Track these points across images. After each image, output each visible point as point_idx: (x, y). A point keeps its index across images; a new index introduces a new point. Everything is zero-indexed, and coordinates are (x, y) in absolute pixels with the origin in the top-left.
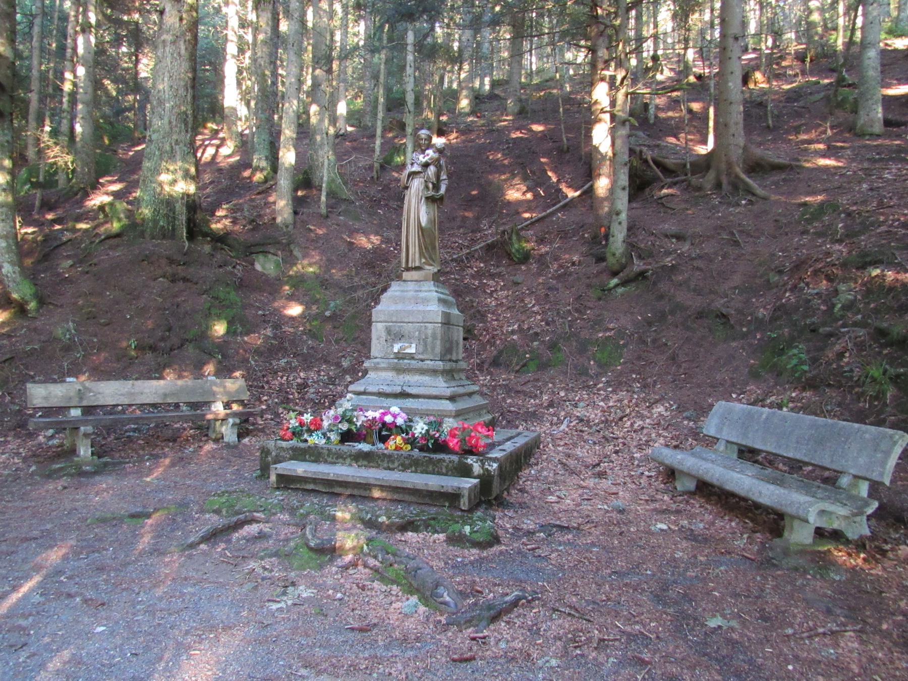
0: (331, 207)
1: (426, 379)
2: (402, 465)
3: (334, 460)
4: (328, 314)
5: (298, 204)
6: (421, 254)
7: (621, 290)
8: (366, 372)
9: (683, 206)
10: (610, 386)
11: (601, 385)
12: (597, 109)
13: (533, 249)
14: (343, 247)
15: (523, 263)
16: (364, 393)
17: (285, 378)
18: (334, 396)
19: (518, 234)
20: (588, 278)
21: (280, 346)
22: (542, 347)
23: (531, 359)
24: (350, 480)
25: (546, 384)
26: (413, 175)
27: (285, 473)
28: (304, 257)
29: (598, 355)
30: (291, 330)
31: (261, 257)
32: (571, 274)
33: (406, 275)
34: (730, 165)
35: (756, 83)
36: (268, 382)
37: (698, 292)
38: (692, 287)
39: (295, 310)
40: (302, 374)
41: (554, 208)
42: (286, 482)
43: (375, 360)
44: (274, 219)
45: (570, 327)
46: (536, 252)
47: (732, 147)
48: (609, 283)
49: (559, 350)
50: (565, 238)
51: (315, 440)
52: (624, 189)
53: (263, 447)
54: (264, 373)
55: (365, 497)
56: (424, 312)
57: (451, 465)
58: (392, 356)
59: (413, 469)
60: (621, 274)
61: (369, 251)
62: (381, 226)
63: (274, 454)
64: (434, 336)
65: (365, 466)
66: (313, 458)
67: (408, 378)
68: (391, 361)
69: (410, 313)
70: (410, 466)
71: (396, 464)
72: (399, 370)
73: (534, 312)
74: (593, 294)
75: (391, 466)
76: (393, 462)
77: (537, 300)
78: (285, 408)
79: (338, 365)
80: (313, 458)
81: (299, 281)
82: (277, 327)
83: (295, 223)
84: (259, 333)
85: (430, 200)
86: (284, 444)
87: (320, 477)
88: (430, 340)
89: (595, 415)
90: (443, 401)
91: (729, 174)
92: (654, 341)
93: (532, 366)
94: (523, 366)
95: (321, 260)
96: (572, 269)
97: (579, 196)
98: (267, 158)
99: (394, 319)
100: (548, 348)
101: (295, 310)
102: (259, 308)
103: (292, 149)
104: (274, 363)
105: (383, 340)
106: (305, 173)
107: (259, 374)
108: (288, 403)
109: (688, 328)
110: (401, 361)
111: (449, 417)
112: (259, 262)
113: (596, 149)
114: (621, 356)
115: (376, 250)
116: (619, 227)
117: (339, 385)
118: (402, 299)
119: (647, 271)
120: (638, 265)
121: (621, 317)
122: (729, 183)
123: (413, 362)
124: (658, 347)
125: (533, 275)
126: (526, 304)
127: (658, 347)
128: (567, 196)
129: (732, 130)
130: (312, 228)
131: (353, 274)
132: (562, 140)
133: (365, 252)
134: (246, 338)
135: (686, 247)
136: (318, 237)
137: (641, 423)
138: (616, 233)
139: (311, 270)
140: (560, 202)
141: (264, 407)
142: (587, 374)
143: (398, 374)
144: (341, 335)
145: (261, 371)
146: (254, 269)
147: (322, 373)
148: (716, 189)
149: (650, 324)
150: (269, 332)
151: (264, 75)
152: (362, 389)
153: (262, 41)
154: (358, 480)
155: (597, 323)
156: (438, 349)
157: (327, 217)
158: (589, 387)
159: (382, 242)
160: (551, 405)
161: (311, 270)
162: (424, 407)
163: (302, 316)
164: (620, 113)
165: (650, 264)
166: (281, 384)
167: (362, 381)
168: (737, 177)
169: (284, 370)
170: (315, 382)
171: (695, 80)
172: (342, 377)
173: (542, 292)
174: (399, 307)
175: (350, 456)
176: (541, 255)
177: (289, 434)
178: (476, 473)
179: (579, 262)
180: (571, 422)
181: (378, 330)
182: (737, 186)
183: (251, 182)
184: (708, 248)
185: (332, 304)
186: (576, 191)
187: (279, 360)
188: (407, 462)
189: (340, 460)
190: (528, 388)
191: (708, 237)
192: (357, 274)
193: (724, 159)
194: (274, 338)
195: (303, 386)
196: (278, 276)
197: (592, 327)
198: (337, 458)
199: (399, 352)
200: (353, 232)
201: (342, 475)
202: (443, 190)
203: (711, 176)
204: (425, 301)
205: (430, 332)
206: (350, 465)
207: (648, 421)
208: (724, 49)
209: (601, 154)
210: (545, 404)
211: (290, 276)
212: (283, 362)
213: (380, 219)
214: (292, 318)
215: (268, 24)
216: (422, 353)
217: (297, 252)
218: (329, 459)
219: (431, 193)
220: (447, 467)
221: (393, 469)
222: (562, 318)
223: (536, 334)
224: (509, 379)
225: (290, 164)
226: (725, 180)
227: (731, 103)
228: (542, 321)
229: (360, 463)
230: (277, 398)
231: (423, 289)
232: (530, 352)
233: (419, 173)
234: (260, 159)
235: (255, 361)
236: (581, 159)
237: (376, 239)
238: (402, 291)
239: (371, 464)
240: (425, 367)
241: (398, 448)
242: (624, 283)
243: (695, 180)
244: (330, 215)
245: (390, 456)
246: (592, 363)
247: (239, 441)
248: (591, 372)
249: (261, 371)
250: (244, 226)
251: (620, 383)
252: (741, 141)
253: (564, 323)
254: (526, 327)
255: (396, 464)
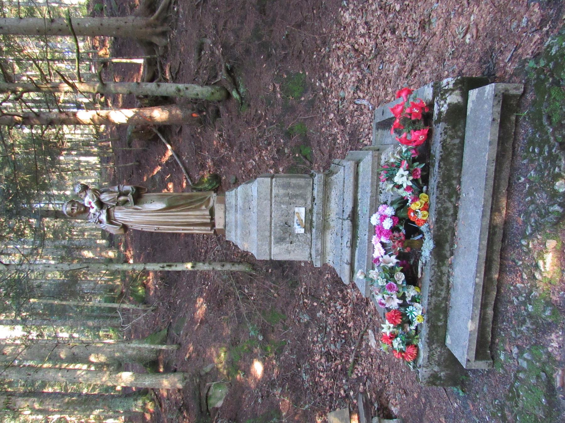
0: (173, 342)
1: (334, 194)
2: (450, 196)
3: (444, 288)
4: (261, 338)
5: (170, 370)
6: (197, 208)
7: (242, 90)
8: (325, 265)
9: (178, 56)
10: (324, 75)
11: (323, 85)
12: (98, 119)
13: (210, 171)
14: (204, 328)
15: (221, 179)
16: (352, 265)
17: (321, 374)
18: (337, 325)
19: (198, 185)
20: (232, 120)
21: (290, 379)
22: (289, 144)
23: (300, 152)
24: (484, 254)
25: (322, 134)
26: (110, 219)
27: (474, 347)
28: (212, 361)
29: (296, 94)
30: (276, 371)
31: (211, 401)
32: (229, 136)
33: (219, 225)
34: (148, 25)
35: (106, 54)
36: (326, 391)
37: (244, 18)
38: (239, 26)
39: (258, 368)
40: (317, 358)
41: (179, 162)
42: (485, 346)
43: (313, 253)
44: (179, 390)
45: (272, 124)
46: (212, 170)
47: (135, 23)
48: (236, 99)
49: (292, 129)
50: (201, 148)
51: (417, 313)
52: (159, 86)
53: (428, 382)
54: (317, 395)
55: (505, 236)
56: (259, 198)
57: (450, 132)
58: (309, 236)
59: (454, 182)
60: (229, 89)
61: (208, 306)
62: (189, 300)
63: (436, 369)
64: (286, 186)
65: (452, 245)
66: (442, 316)
67: (333, 216)
68: (314, 236)
69: (260, 214)
70: (450, 186)
71: (449, 205)
72: (324, 227)
73: (259, 159)
74: (245, 111)
75: (451, 212)
76: (447, 209)
77: (250, 158)
78: (352, 372)
79: (307, 325)
80: (442, 316)
81: (233, 365)
82: (272, 385)
83: (183, 372)
84: (279, 401)
85: (138, 198)
86: (423, 355)
87: (480, 297)
88: (290, 191)
89: (352, 77)
90: (361, 169)
91: (155, 26)
92: (284, 48)
93: (306, 151)
94: (305, 157)
95: (214, 346)
96: (225, 136)
97: (171, 146)
98: (136, 400)
99: (267, 234)
100: (290, 139)
101: (258, 368)
102: (256, 401)
103: (119, 374)
104: (306, 385)
105: (291, 247)
106: (145, 365)
107: (318, 400)
108: (346, 369)
109: (273, 21)
110: (314, 224)
111: (379, 159)
112: (214, 404)
113: (130, 120)
114: (298, 74)
115: (207, 301)
116: (190, 89)
117: (326, 322)
118: (245, 227)
119: (226, 68)
120: (222, 76)
121: (266, 82)
122: (162, 25)
123: (315, 211)
124: (289, 43)
125: (229, 168)
126: (253, 167)
127: (289, 43)
128: (171, 156)
129: (123, 24)
130: (188, 356)
131: (226, 317)
132: (132, 166)
133: (209, 308)
134: (284, 414)
135: (208, 41)
136: (195, 350)
137: (361, 27)
138: (195, 92)
139: (222, 355)
140: (175, 160)
141: (352, 393)
142: (313, 101)
143: (329, 228)
144: (280, 325)
145: (315, 398)
146: (221, 407)
147: (315, 339)
148: (166, 35)
149: (269, 56)
150: (278, 391)
151: (68, 403)
152: (347, 268)
153: (40, 405)
154: (485, 243)
155: (269, 102)
156: (302, 182)
157: (180, 344)
158: (325, 95)
159: (201, 296)
160: (342, 122)
161: (222, 355)
162: (368, 190)
163: (263, 361)
164: (96, 88)
165: (221, 65)
166: (327, 377)
167: (338, 270)
168: (157, 19)
169: (313, 375)
170: (324, 346)
171: (104, 97)
172: (319, 320)
173: (243, 154)
174: (253, 228)
175: (439, 266)
176: (214, 165)
177: (411, 350)
178: (460, 99)
179: (219, 131)
180: (359, 98)
181: (279, 253)
182: (164, 20)
183: (154, 413)
184: (209, 22)
185: (252, 333)
186: (167, 148)
187: (303, 381)
188: (446, 191)
189: (445, 278)
190: (326, 149)
191: (200, 25)
192: (227, 314)
193: (144, 30)
194: (283, 387)
195: (328, 356)
196: (227, 385)
197: (272, 105)
198: (442, 284)
199: (305, 227)
200: (193, 321)
201: (478, 266)
202: (128, 188)
203: (156, 40)
204: (247, 199)
205: (282, 192)
206: (451, 266)
207: (358, 22)
208: (60, 30)
209: (135, 115)
210: (342, 128)
211: (228, 374)
212: (306, 377)
213: (185, 301)
214: (265, 370)
215: (27, 400)
216: (306, 200)
217: (208, 369)
218: (443, 294)
219: (130, 198)
220: (452, 138)
221: (456, 209)
222: (264, 133)
223: (278, 151)
224: (318, 168)
225: (132, 376)
226: (160, 29)
227: (101, 25)
228: (267, 149)
229: (448, 254)
230: (342, 380)
231: (234, 202)
232: (294, 154)
233: (108, 212)
234: (136, 405)
235: (305, 404)
236: (145, 150)
237: (200, 301)
238: (236, 226)
239: (449, 238)
240: (321, 195)
241: (426, 207)
242: (236, 86)
243: (161, 50)
244: (178, 342)
245: (440, 214)
246: (303, 99)
247: (396, 418)
248: (311, 97)
249: (315, 398)
250: (184, 417)
251: (322, 67)
252: (131, 18)
253: (269, 130)
254: (272, 162)
255: (449, 205)
